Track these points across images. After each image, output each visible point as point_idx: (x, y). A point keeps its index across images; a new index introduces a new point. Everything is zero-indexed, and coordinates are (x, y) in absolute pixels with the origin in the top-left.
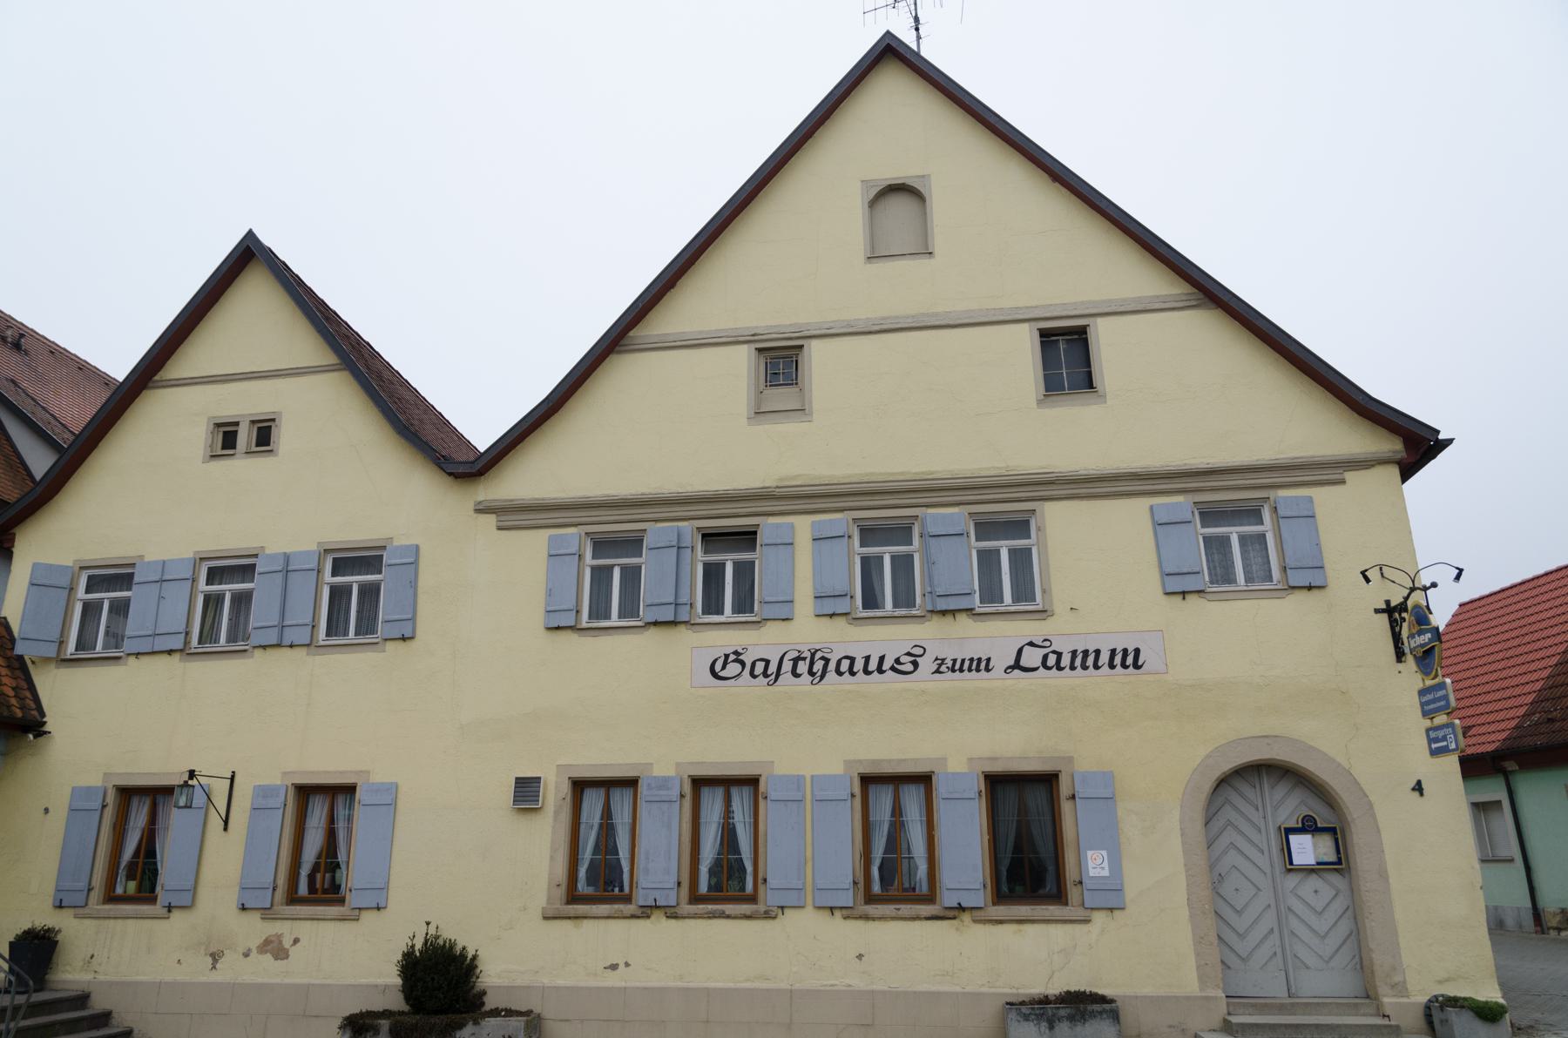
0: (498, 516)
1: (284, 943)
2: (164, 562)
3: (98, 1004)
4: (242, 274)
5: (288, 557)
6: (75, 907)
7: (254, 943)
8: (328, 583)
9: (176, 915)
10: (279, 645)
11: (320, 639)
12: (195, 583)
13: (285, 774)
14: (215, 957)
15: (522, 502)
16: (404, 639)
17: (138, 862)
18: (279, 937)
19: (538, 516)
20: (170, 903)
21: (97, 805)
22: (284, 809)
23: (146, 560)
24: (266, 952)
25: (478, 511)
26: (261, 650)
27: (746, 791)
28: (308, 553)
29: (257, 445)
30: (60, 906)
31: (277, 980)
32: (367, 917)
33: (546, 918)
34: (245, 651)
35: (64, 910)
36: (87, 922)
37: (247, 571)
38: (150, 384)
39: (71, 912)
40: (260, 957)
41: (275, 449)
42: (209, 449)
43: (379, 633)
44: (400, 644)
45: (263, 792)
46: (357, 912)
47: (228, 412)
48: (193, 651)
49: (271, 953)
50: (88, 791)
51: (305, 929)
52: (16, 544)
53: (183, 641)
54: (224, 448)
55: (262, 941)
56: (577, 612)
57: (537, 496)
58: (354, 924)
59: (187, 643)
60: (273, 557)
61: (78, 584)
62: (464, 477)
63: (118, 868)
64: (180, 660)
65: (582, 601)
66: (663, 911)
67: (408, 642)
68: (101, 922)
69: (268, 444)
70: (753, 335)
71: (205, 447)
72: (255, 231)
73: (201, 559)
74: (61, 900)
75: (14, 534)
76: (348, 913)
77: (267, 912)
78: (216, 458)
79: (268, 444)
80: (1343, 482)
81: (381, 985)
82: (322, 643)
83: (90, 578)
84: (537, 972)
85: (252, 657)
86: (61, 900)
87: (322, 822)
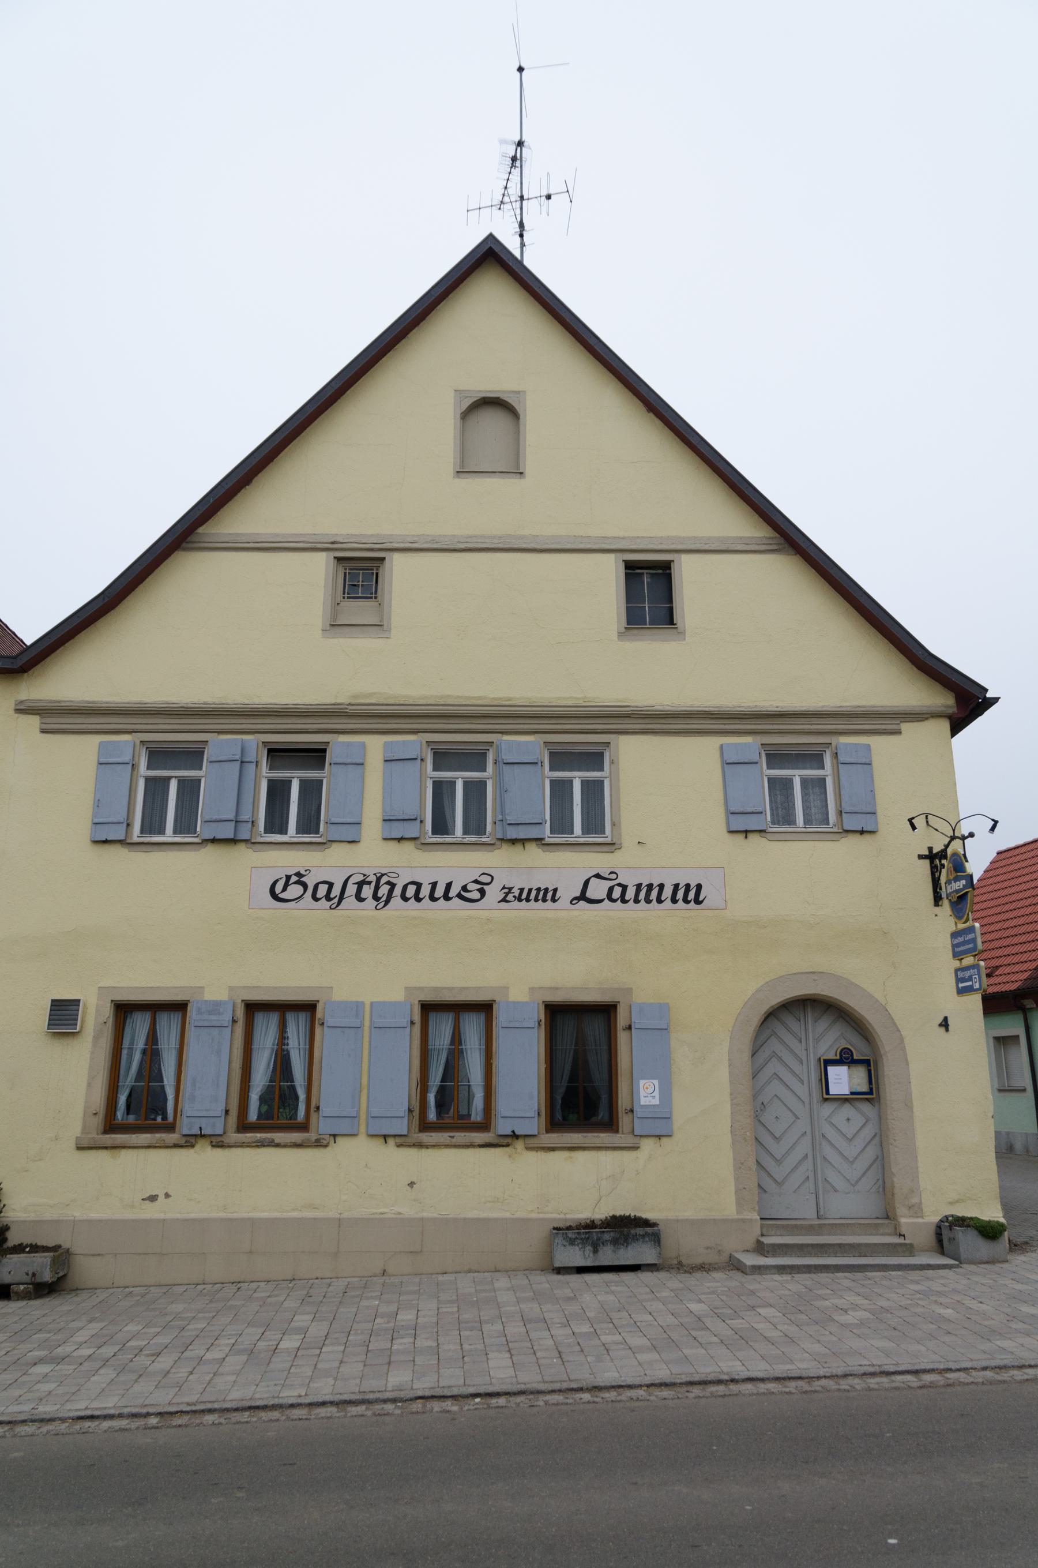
0: (42, 718)
25: (19, 711)
27: (303, 1017)
33: (80, 1148)
38: (184, 545)
57: (87, 699)
70: (332, 543)
80: (898, 732)
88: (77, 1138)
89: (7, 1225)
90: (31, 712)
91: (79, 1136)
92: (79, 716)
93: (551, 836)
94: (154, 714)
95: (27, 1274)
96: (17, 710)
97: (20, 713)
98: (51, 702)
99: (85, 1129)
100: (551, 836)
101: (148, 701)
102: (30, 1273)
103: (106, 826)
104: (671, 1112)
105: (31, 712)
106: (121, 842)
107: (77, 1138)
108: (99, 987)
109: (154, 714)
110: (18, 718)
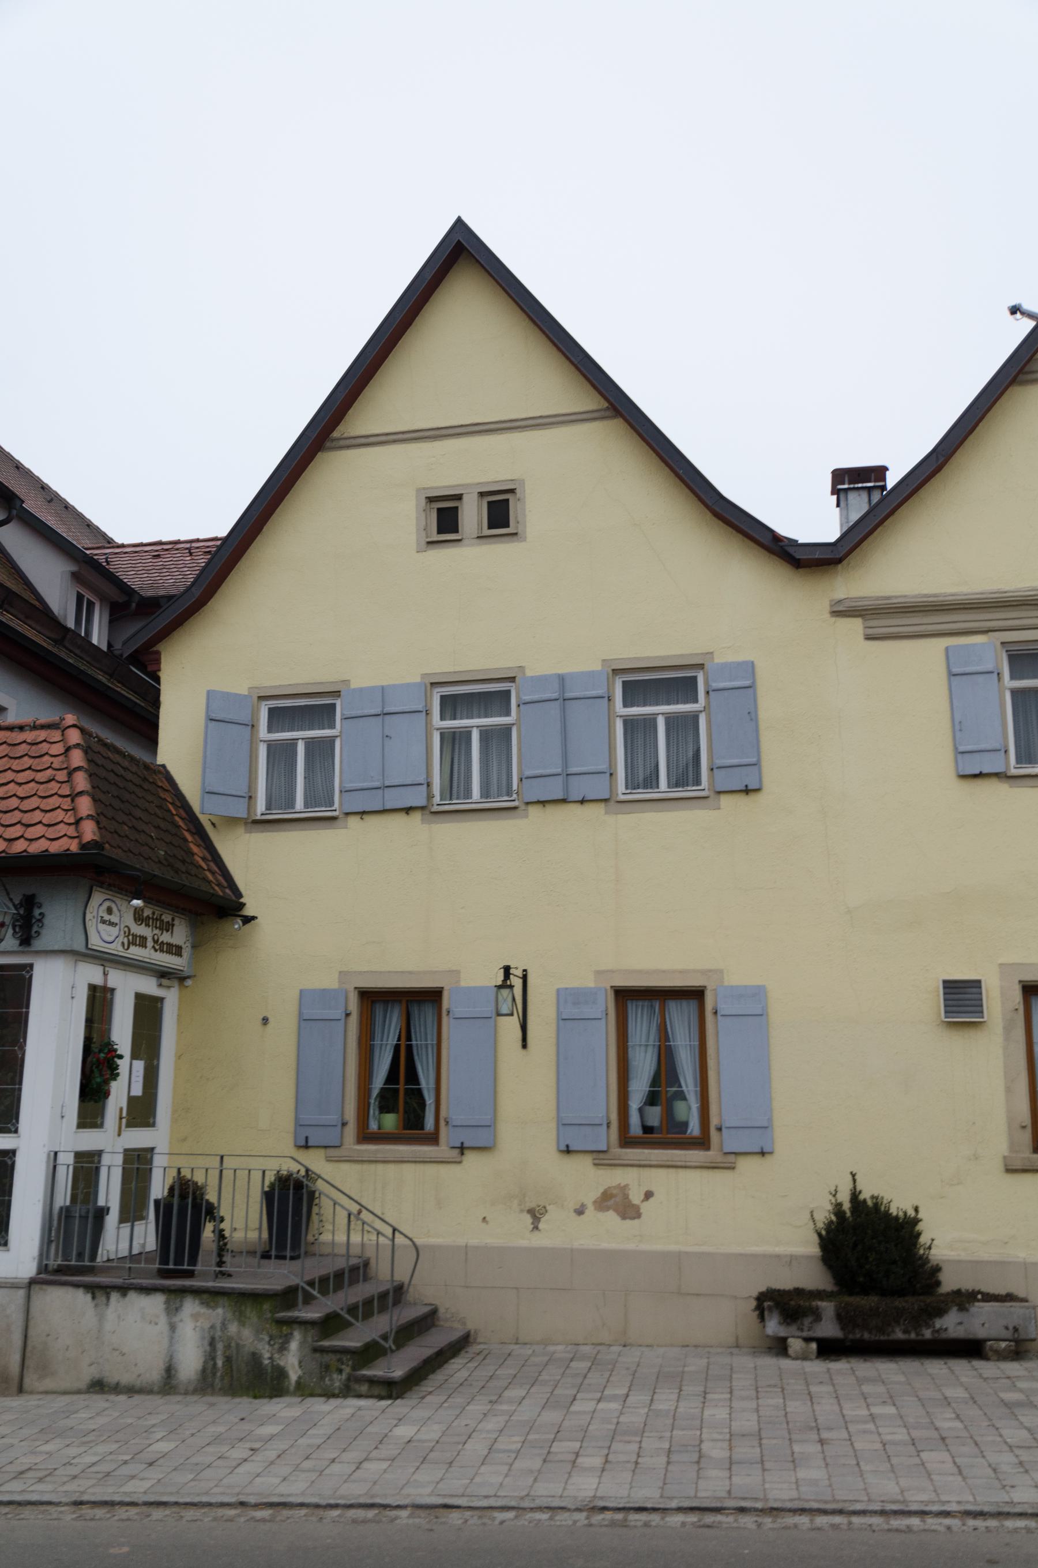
0: (865, 620)
1: (631, 1197)
2: (383, 687)
3: (383, 1274)
4: (444, 281)
5: (563, 679)
6: (326, 1147)
7: (589, 1197)
8: (621, 716)
9: (471, 1159)
10: (564, 801)
11: (620, 792)
12: (611, 703)
13: (598, 973)
14: (536, 1215)
15: (903, 600)
16: (747, 791)
17: (397, 1091)
18: (624, 1189)
19: (925, 620)
20: (462, 1143)
21: (339, 1014)
22: (607, 1018)
23: (353, 686)
24: (608, 1209)
25: (836, 614)
26: (539, 807)
27: (689, 1007)
28: (591, 674)
29: (490, 527)
30: (306, 1146)
31: (631, 1246)
32: (747, 1166)
33: (1010, 1170)
34: (515, 808)
35: (311, 1151)
36: (345, 1167)
37: (499, 701)
38: (328, 444)
39: (321, 1153)
40: (602, 1216)
41: (520, 531)
42: (423, 534)
43: (336, 805)
44: (741, 800)
45: (567, 997)
46: (731, 1158)
47: (444, 481)
48: (435, 808)
49: (616, 1210)
50: (324, 995)
51: (658, 1179)
52: (163, 666)
53: (425, 794)
54: (440, 531)
55: (599, 1194)
56: (611, 774)
57: (925, 592)
58: (727, 1174)
59: (430, 796)
60: (542, 680)
61: (258, 720)
62: (810, 567)
63: (369, 1097)
64: (422, 820)
65: (256, 778)
66: (322, 1152)
67: (753, 797)
68: (365, 1167)
69: (507, 525)
71: (418, 530)
72: (464, 218)
73: (432, 684)
74: (307, 1138)
75: (158, 653)
76: (720, 1158)
77: (601, 1156)
78: (436, 545)
79: (507, 525)
81: (786, 1256)
82: (622, 798)
83: (272, 711)
84: (1006, 1243)
85: (527, 816)
86: (307, 1138)
87: (652, 1037)
88: (1005, 1157)
89: (937, 1265)
90: (851, 613)
91: (1006, 1154)
92: (913, 614)
93: (1018, 766)
94: (1017, 605)
95: (1007, 1328)
96: (834, 612)
97: (837, 616)
98: (878, 598)
99: (1012, 1146)
100: (1018, 766)
101: (1007, 589)
102: (1011, 1328)
103: (977, 755)
104: (770, 1120)
105: (851, 613)
106: (997, 775)
107: (1005, 1157)
108: (1001, 965)
109: (1017, 605)
110: (835, 622)
